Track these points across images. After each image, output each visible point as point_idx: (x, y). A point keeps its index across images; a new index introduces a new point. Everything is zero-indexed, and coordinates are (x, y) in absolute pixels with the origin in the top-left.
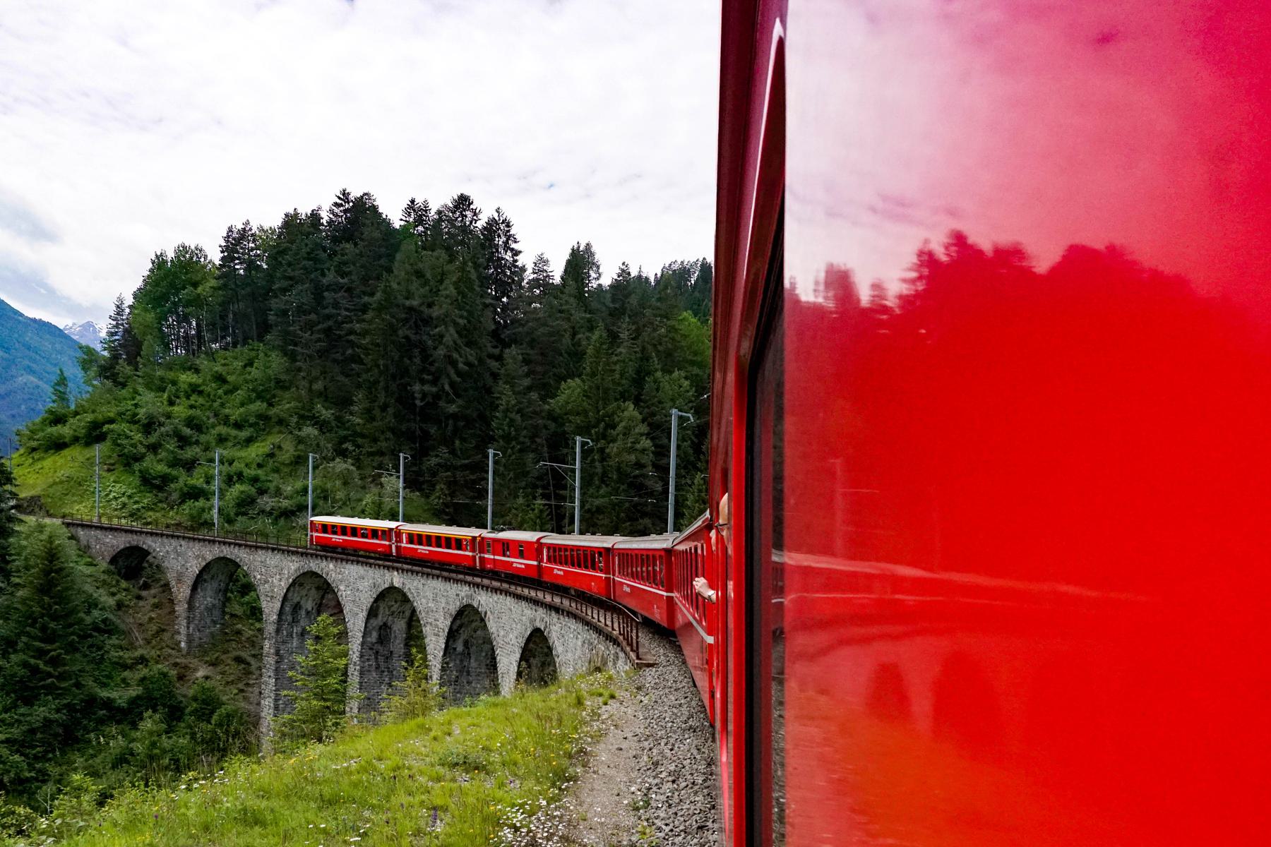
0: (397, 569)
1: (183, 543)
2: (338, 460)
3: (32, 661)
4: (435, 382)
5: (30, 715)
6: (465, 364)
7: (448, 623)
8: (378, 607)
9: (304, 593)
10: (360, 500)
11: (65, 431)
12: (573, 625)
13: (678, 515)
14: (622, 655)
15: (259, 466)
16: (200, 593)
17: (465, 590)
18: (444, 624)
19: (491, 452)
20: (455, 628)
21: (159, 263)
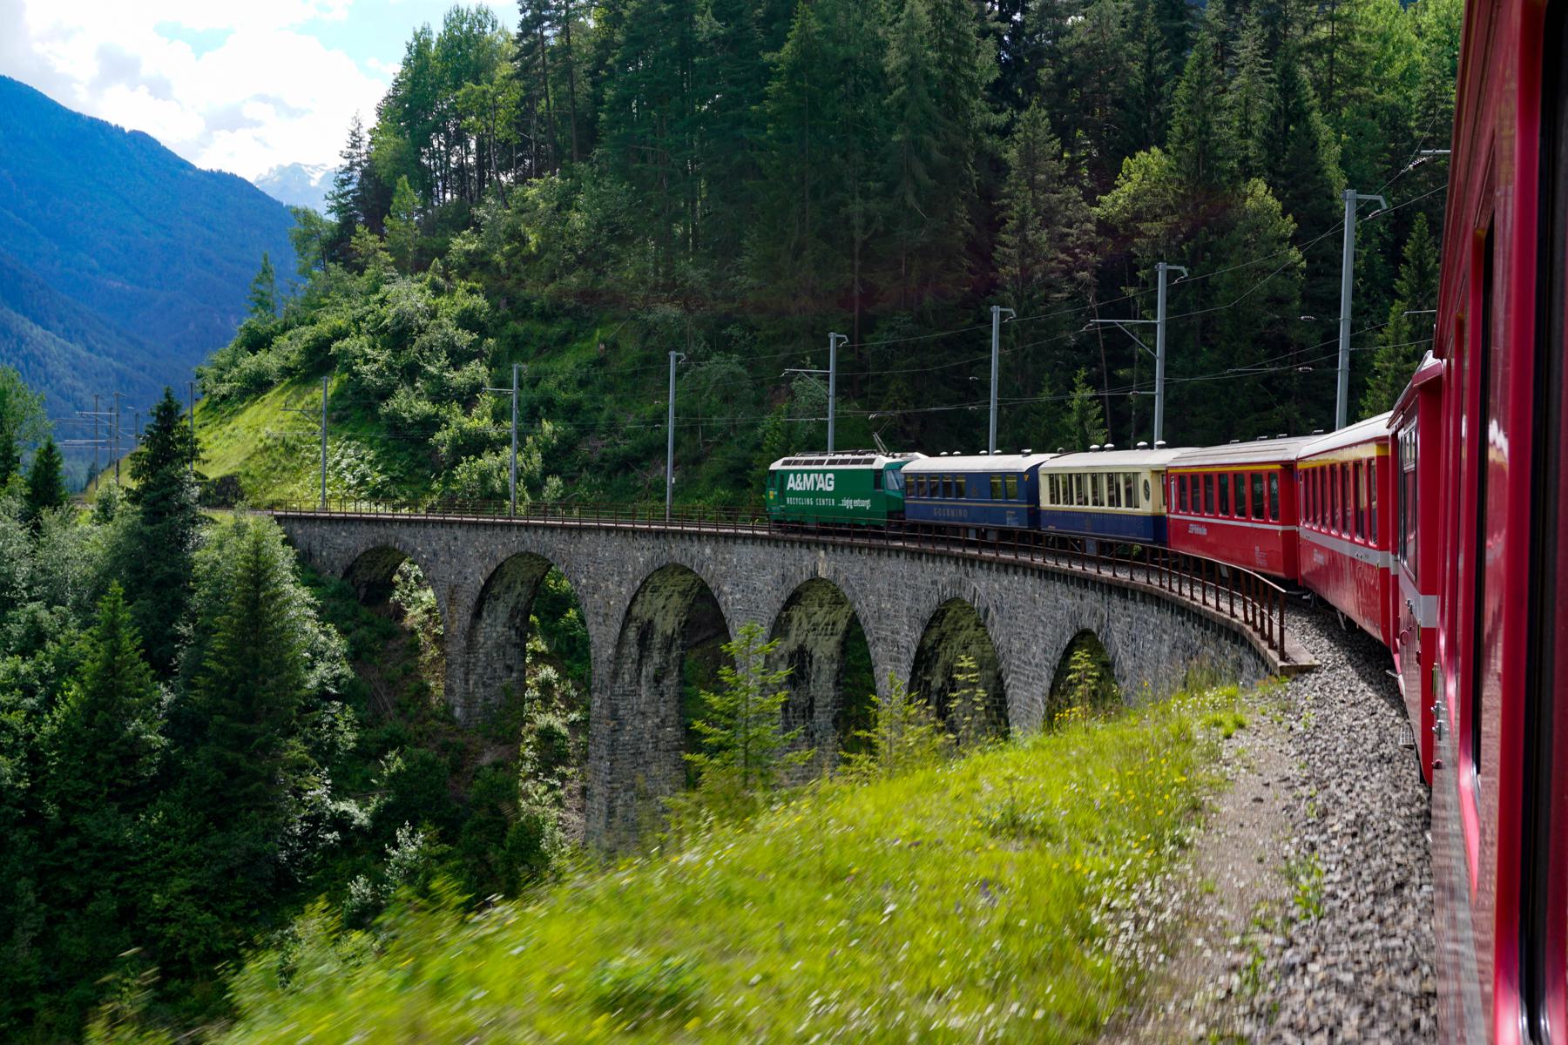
0: (825, 546)
1: (459, 533)
2: (715, 358)
3: (230, 755)
4: (887, 193)
5: (226, 846)
6: (943, 151)
7: (917, 635)
8: (789, 619)
9: (660, 602)
10: (753, 426)
11: (269, 360)
12: (1154, 616)
13: (1357, 389)
14: (1249, 660)
15: (582, 384)
16: (487, 620)
17: (948, 572)
18: (909, 637)
19: (996, 310)
20: (929, 643)
21: (419, 52)
